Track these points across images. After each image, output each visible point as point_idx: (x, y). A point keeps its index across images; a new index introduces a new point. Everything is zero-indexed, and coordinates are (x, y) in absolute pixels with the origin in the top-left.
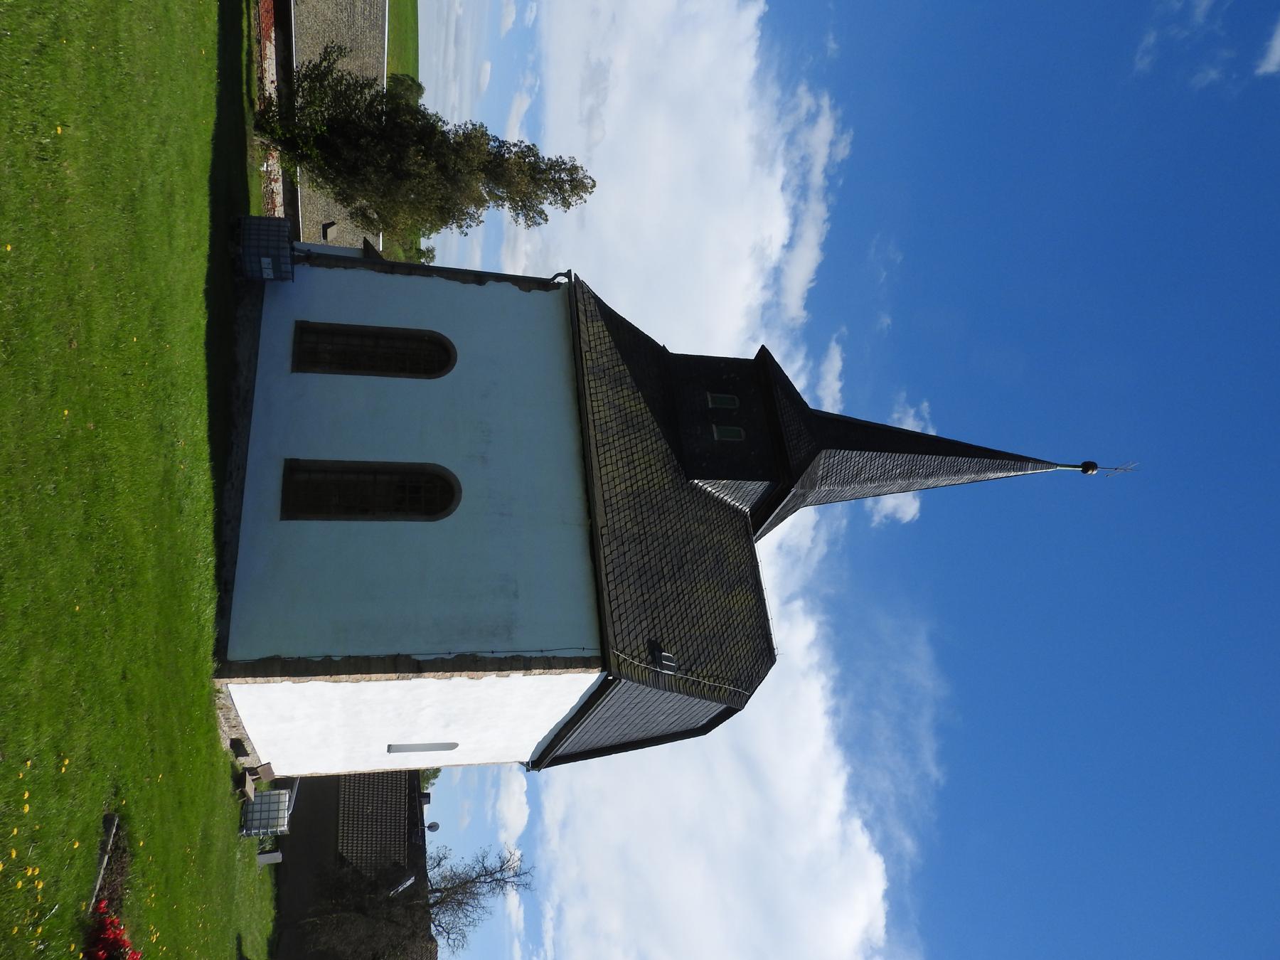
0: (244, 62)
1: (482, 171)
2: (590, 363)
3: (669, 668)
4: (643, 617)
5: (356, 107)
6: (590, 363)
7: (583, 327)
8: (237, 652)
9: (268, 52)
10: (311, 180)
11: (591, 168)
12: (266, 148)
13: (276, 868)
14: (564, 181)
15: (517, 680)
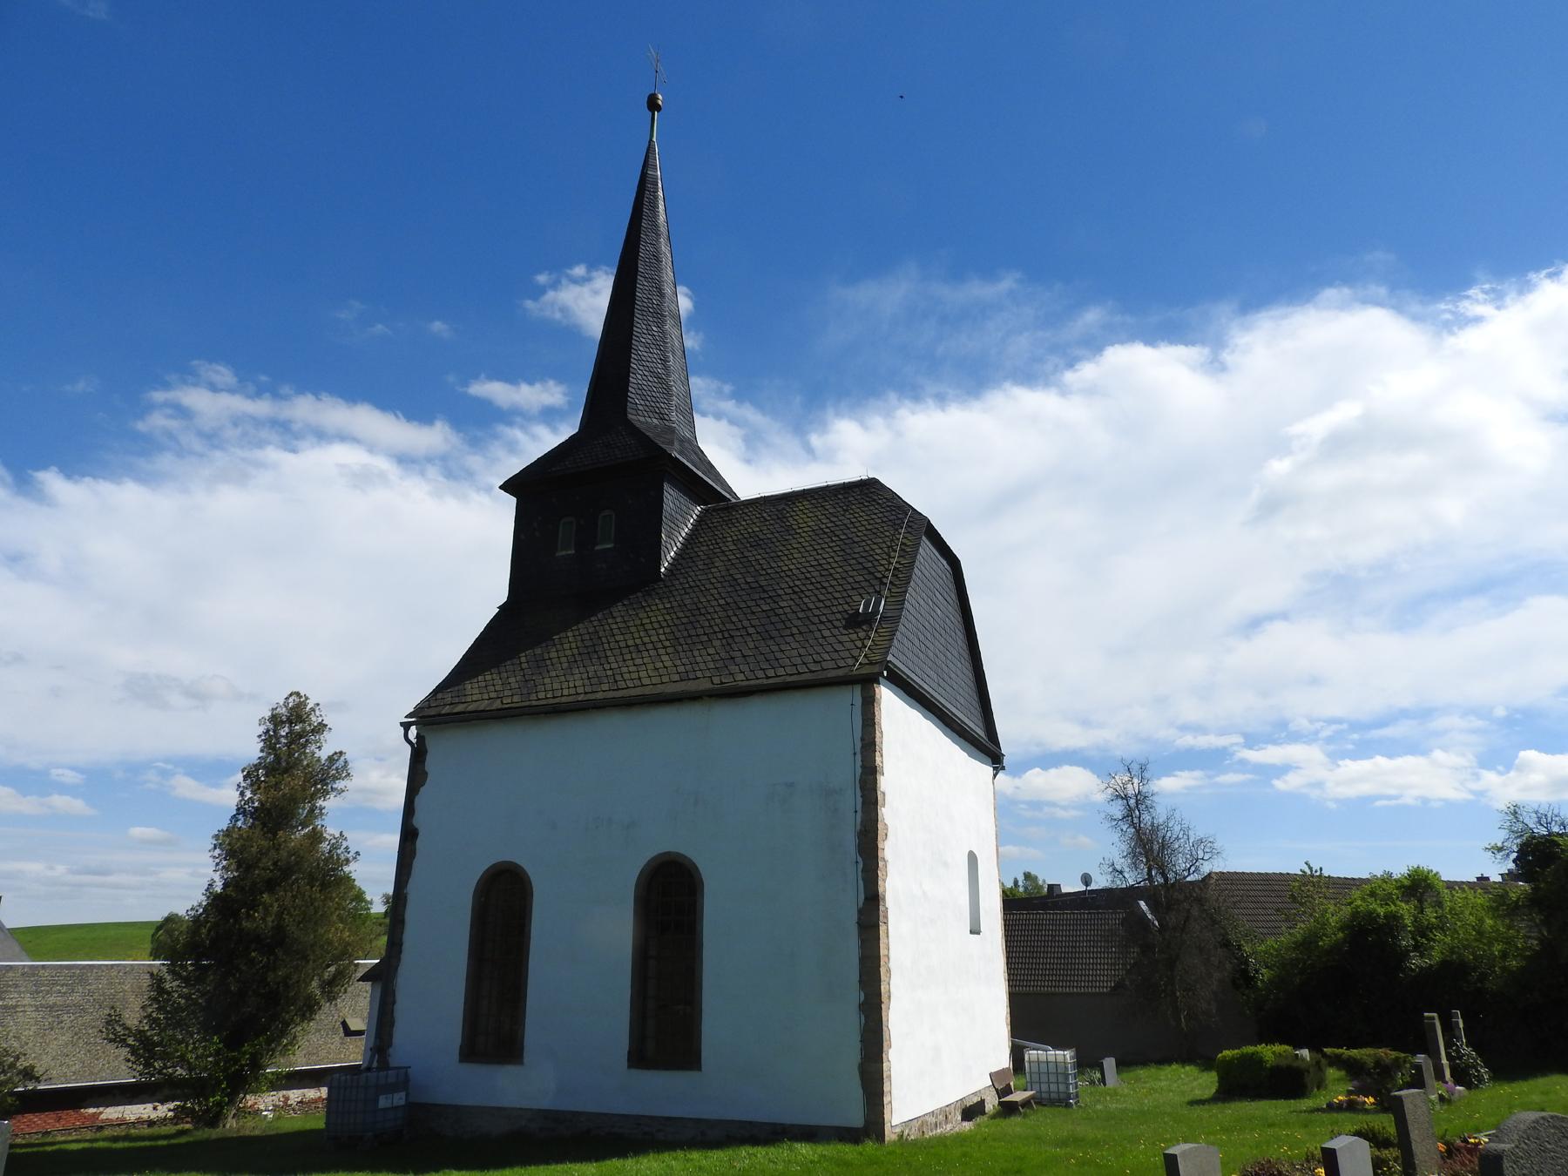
0: (127, 1144)
1: (275, 834)
2: (516, 699)
3: (877, 604)
4: (818, 634)
5: (187, 997)
6: (516, 699)
7: (472, 707)
8: (856, 1119)
9: (114, 1116)
10: (285, 1051)
11: (275, 697)
12: (242, 1113)
13: (1122, 1065)
14: (291, 732)
15: (888, 783)
